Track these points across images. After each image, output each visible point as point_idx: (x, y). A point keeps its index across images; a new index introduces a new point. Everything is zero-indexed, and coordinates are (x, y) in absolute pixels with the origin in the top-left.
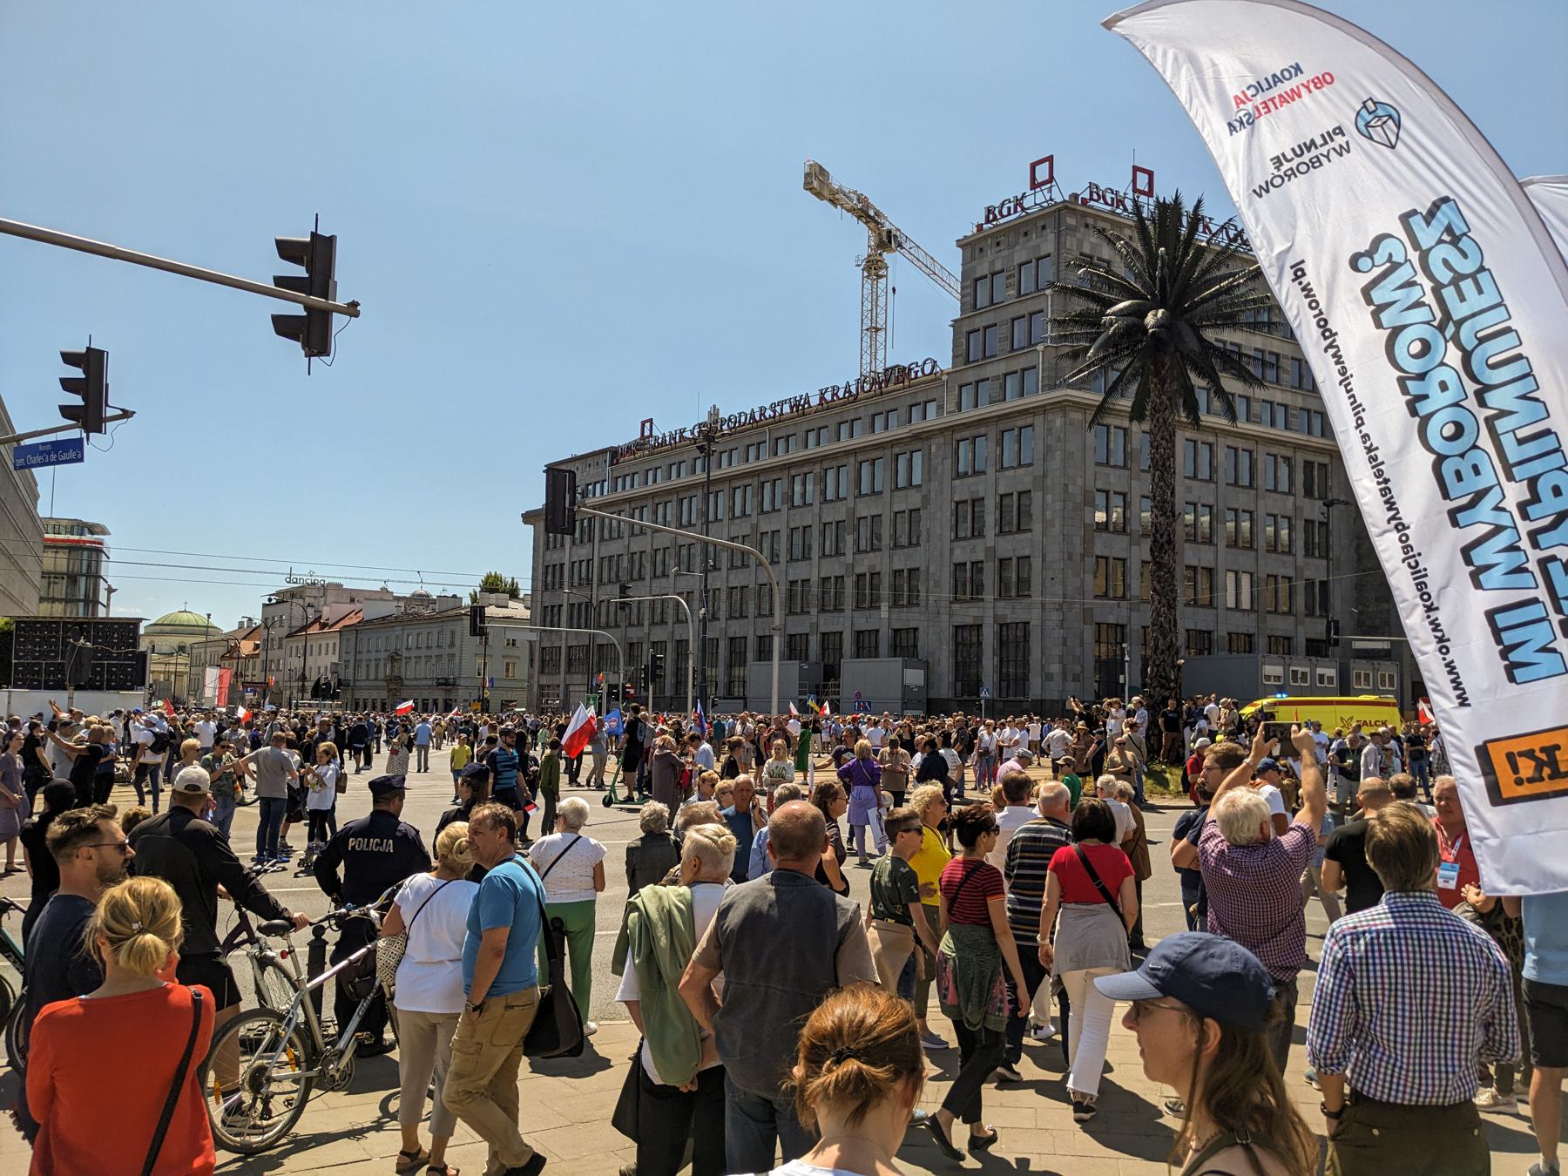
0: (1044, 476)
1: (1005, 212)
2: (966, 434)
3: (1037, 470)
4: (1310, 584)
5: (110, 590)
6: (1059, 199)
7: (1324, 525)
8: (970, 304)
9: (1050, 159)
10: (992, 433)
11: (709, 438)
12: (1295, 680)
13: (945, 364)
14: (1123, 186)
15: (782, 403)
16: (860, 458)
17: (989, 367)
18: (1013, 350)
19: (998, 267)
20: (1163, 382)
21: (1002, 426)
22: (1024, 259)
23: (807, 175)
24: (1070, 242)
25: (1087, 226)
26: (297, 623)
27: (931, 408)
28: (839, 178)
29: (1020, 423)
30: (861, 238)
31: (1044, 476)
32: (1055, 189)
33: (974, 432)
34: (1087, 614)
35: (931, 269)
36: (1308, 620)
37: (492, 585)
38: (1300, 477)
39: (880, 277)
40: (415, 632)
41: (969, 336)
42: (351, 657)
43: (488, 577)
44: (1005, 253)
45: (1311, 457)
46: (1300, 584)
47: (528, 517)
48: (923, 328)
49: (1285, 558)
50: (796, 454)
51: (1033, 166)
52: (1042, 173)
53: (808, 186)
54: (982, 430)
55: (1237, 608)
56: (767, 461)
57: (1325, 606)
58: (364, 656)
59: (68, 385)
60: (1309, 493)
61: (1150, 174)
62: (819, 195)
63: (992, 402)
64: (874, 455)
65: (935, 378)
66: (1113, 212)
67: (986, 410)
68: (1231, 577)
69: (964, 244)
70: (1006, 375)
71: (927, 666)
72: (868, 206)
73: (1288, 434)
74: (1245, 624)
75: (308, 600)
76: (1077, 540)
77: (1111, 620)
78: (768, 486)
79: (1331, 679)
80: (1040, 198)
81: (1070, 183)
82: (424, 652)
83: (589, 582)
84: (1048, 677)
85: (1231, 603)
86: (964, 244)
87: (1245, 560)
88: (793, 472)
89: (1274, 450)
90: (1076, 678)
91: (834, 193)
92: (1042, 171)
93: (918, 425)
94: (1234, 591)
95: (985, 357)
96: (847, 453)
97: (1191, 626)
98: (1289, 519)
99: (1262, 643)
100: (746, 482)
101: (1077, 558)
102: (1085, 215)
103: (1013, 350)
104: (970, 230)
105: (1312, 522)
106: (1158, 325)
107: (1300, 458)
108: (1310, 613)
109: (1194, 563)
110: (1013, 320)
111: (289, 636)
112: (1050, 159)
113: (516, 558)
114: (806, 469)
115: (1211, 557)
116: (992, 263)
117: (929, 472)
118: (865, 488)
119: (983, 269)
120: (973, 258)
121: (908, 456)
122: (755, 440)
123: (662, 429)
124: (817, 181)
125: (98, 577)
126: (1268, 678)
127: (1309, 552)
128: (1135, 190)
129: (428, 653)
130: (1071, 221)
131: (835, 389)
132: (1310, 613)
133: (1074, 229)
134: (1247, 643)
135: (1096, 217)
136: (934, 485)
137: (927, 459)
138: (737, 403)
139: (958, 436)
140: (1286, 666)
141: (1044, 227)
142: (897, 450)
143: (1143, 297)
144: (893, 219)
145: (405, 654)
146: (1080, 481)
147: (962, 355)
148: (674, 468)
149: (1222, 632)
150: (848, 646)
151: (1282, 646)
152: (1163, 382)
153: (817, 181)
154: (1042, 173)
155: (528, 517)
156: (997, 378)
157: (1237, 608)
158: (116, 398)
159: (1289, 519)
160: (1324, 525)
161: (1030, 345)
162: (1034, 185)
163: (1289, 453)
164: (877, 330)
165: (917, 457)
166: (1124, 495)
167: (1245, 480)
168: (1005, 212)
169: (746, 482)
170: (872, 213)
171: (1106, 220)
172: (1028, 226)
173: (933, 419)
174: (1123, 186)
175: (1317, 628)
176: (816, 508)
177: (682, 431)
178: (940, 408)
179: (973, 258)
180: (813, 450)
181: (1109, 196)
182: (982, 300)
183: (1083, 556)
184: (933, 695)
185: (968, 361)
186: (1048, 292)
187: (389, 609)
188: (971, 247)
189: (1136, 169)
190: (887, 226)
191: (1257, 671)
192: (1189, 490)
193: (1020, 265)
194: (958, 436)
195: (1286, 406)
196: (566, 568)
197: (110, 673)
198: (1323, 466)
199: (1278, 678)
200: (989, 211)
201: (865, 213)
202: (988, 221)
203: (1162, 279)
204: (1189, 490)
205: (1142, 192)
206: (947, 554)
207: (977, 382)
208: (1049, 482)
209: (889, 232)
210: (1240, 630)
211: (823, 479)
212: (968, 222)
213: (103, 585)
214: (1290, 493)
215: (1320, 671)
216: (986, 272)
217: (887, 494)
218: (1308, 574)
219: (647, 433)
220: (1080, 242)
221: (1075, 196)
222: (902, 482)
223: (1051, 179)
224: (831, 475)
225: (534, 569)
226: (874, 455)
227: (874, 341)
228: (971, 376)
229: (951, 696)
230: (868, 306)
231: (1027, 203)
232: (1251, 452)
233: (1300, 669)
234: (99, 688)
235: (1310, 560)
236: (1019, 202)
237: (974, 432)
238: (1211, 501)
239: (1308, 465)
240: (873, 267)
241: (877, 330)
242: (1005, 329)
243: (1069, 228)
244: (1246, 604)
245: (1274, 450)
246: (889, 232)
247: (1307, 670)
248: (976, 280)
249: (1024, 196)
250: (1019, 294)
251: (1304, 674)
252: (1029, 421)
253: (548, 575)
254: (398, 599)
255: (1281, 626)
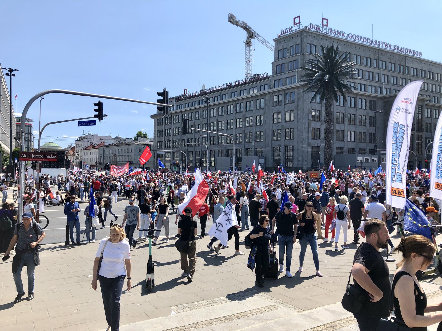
0: (298, 106)
1: (287, 31)
2: (276, 94)
3: (296, 104)
4: (371, 134)
5: (34, 137)
6: (302, 28)
7: (375, 117)
8: (277, 58)
9: (299, 17)
10: (283, 93)
11: (204, 93)
12: (366, 161)
13: (270, 74)
14: (319, 23)
15: (224, 85)
16: (246, 101)
17: (282, 75)
18: (289, 71)
19: (285, 47)
20: (329, 92)
21: (286, 92)
22: (292, 45)
23: (229, 18)
24: (305, 40)
25: (309, 36)
26: (86, 146)
27: (266, 86)
28: (239, 18)
29: (291, 91)
30: (244, 34)
31: (298, 106)
32: (300, 25)
33: (279, 94)
34: (309, 143)
35: (264, 42)
36: (370, 144)
37: (139, 135)
38: (368, 105)
39: (250, 46)
40: (120, 149)
41: (277, 67)
42: (102, 155)
43: (139, 132)
44: (287, 43)
45: (371, 99)
46: (368, 134)
47: (152, 117)
48: (264, 63)
49: (364, 127)
50: (228, 100)
51: (294, 19)
52: (297, 21)
53: (230, 21)
54: (281, 93)
55: (351, 141)
56: (220, 101)
57: (375, 140)
58: (106, 155)
59: (95, 110)
60: (371, 109)
61: (327, 20)
62: (233, 23)
63: (283, 86)
64: (250, 100)
65: (267, 78)
66: (316, 31)
67: (282, 88)
68: (349, 133)
69: (275, 40)
70: (287, 78)
71: (265, 158)
72: (247, 26)
73: (366, 93)
74: (352, 146)
75: (88, 139)
76: (307, 124)
77: (316, 145)
78: (220, 108)
79: (375, 161)
80: (296, 28)
81: (305, 23)
82: (123, 154)
83: (170, 134)
84: (299, 161)
85: (349, 140)
86: (275, 40)
87: (353, 128)
88: (228, 104)
89: (361, 97)
90: (306, 161)
91: (237, 22)
92: (297, 20)
93: (262, 92)
94: (350, 136)
95: (281, 72)
96: (243, 99)
97: (338, 146)
98: (365, 116)
99: (357, 151)
100: (214, 107)
101: (307, 128)
102: (309, 32)
103: (289, 71)
104: (277, 37)
105: (372, 117)
106: (329, 79)
107: (368, 99)
108: (371, 142)
109: (339, 129)
110: (289, 62)
111: (84, 149)
112: (299, 17)
113: (149, 128)
114: (231, 104)
115: (343, 127)
116: (283, 46)
117: (266, 104)
118: (248, 109)
119: (281, 48)
120: (278, 45)
121: (259, 100)
122: (217, 95)
123: (191, 92)
124: (232, 20)
125: (31, 134)
126: (358, 160)
127: (371, 125)
128: (323, 25)
129: (127, 154)
130: (305, 34)
131: (239, 81)
132: (371, 142)
133: (306, 37)
134: (352, 151)
135: (312, 33)
136: (267, 108)
137: (265, 101)
138: (210, 85)
139: (274, 95)
140: (363, 157)
141: (297, 36)
142: (257, 98)
143: (325, 71)
144: (254, 28)
145: (118, 155)
146: (307, 107)
147: (275, 72)
148: (194, 103)
149: (346, 148)
150: (243, 153)
151: (362, 152)
152: (329, 92)
153: (232, 20)
154: (297, 21)
155: (152, 117)
156: (284, 79)
157: (351, 141)
158: (104, 113)
159: (365, 116)
160: (375, 117)
161: (294, 69)
162: (295, 24)
163: (430, 108)
164: (249, 61)
165: (262, 100)
166: (320, 111)
167: (353, 106)
168: (287, 31)
169: (214, 107)
170: (248, 28)
171: (314, 34)
172: (292, 36)
173: (267, 90)
174: (319, 23)
175: (372, 146)
176: (234, 114)
177: (196, 92)
178: (269, 86)
179: (278, 45)
180: (233, 99)
181: (316, 27)
182: (281, 56)
183: (308, 128)
184: (267, 166)
185: (276, 74)
186: (299, 54)
187: (112, 142)
188: (277, 41)
189: (323, 19)
190: (252, 31)
191: (355, 159)
192: (338, 109)
193: (291, 47)
194: (274, 95)
195: (365, 85)
196: (163, 131)
197: (58, 164)
198: (375, 101)
199: (361, 160)
200: (282, 31)
201: (246, 28)
202: (282, 34)
203: (328, 67)
204: (338, 109)
205: (325, 25)
206: (271, 127)
207: (279, 80)
208: (299, 107)
209: (253, 33)
210: (352, 147)
211: (236, 107)
212: (276, 34)
213: (32, 136)
214: (365, 109)
215: (372, 158)
216: (281, 48)
217: (254, 111)
218: (370, 131)
219: (186, 93)
220: (308, 40)
221: (306, 27)
222: (258, 107)
223: (300, 22)
224: (238, 105)
225: (154, 131)
226: (250, 100)
227: (248, 65)
228: (277, 78)
229: (272, 166)
230: (247, 54)
231: (293, 29)
232: (355, 98)
233: (367, 158)
234: (56, 168)
235: (371, 128)
236: (290, 29)
237: (279, 94)
238: (344, 112)
239: (371, 101)
240: (248, 43)
241: (249, 61)
242: (287, 64)
243: (305, 36)
244: (353, 140)
245: (361, 97)
246: (253, 33)
247: (369, 158)
248: (279, 51)
249: (292, 27)
250: (291, 55)
251: (368, 159)
252: (294, 91)
253: (158, 133)
254: (113, 139)
255: (362, 145)
